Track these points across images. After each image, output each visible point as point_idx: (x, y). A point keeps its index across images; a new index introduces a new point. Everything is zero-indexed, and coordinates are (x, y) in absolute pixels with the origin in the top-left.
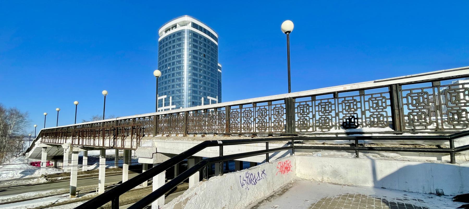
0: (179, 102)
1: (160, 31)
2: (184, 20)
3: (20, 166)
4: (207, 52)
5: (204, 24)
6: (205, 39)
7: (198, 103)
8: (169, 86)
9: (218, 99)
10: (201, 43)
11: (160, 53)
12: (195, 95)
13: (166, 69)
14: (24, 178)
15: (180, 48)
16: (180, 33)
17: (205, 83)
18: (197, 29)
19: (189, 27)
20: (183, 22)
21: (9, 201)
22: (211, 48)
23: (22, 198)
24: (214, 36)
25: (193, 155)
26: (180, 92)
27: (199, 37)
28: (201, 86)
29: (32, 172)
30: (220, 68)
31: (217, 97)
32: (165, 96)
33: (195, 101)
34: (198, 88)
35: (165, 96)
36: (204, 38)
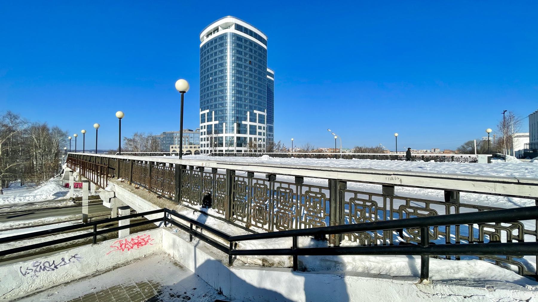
0: (222, 117)
1: (201, 36)
2: (226, 22)
3: (241, 231)
4: (253, 52)
5: (250, 25)
6: (251, 43)
7: (243, 118)
8: (212, 99)
9: (267, 113)
10: (246, 47)
11: (202, 62)
12: (239, 96)
13: (208, 79)
14: (56, 199)
15: (223, 55)
16: (222, 38)
17: (251, 95)
18: (241, 31)
19: (232, 30)
20: (226, 23)
21: (30, 225)
22: (259, 53)
23: (42, 222)
24: (260, 37)
25: (200, 47)
26: (223, 100)
27: (243, 41)
28: (246, 99)
29: (65, 193)
30: (270, 74)
31: (266, 110)
32: (208, 111)
33: (239, 116)
34: (243, 101)
35: (208, 111)
36: (250, 42)
